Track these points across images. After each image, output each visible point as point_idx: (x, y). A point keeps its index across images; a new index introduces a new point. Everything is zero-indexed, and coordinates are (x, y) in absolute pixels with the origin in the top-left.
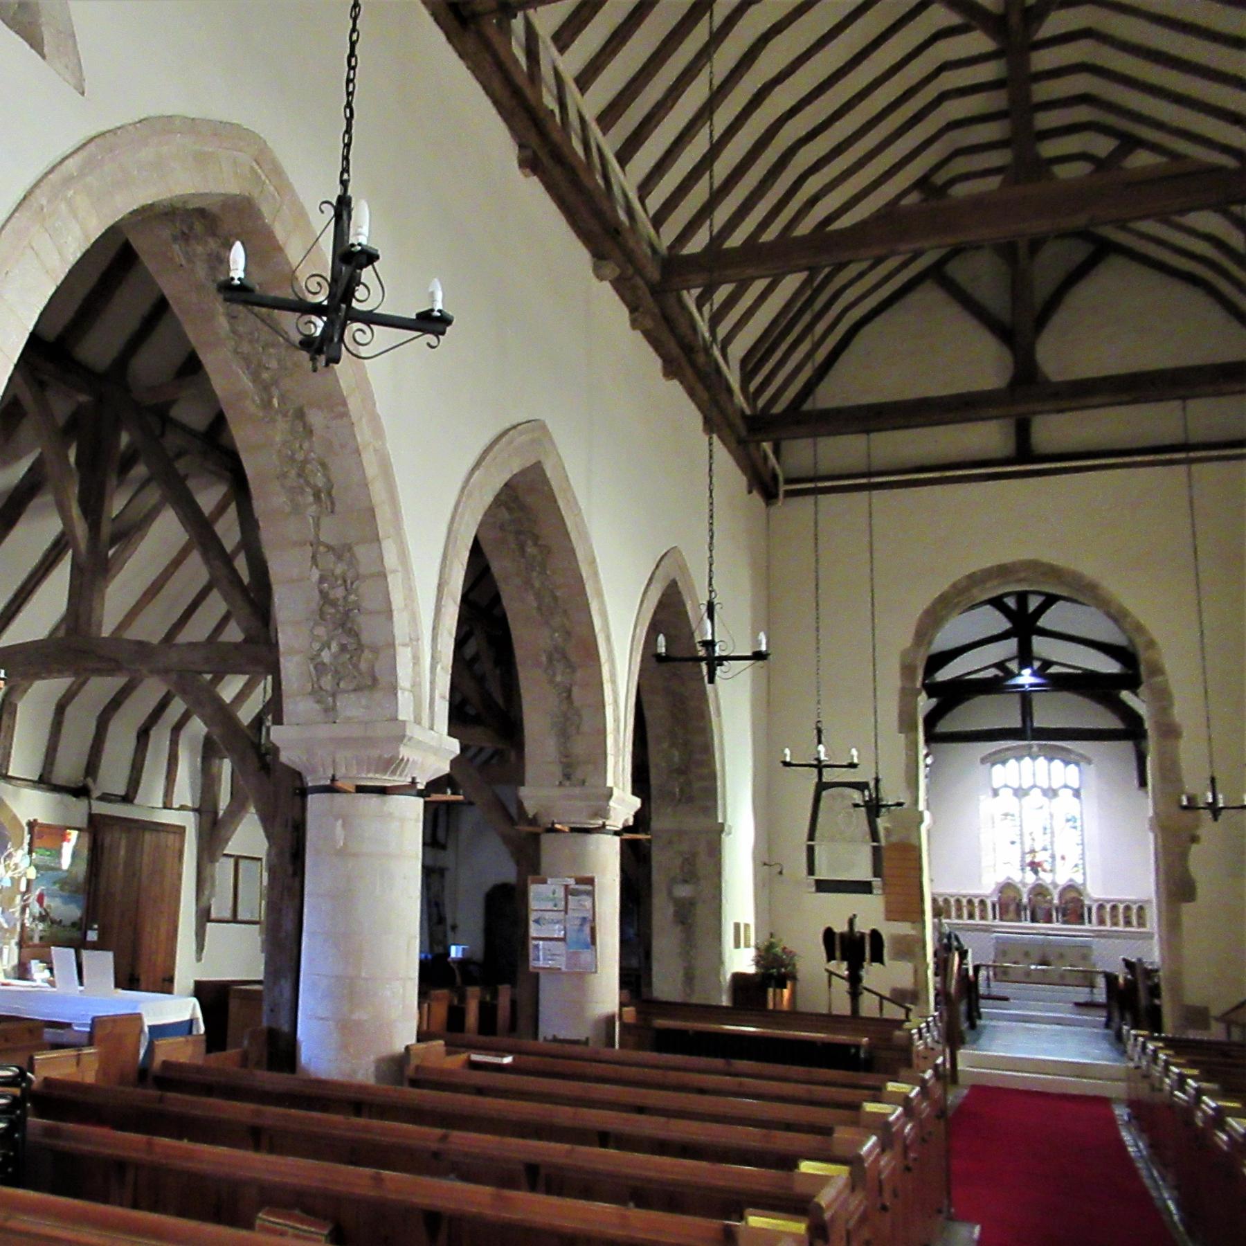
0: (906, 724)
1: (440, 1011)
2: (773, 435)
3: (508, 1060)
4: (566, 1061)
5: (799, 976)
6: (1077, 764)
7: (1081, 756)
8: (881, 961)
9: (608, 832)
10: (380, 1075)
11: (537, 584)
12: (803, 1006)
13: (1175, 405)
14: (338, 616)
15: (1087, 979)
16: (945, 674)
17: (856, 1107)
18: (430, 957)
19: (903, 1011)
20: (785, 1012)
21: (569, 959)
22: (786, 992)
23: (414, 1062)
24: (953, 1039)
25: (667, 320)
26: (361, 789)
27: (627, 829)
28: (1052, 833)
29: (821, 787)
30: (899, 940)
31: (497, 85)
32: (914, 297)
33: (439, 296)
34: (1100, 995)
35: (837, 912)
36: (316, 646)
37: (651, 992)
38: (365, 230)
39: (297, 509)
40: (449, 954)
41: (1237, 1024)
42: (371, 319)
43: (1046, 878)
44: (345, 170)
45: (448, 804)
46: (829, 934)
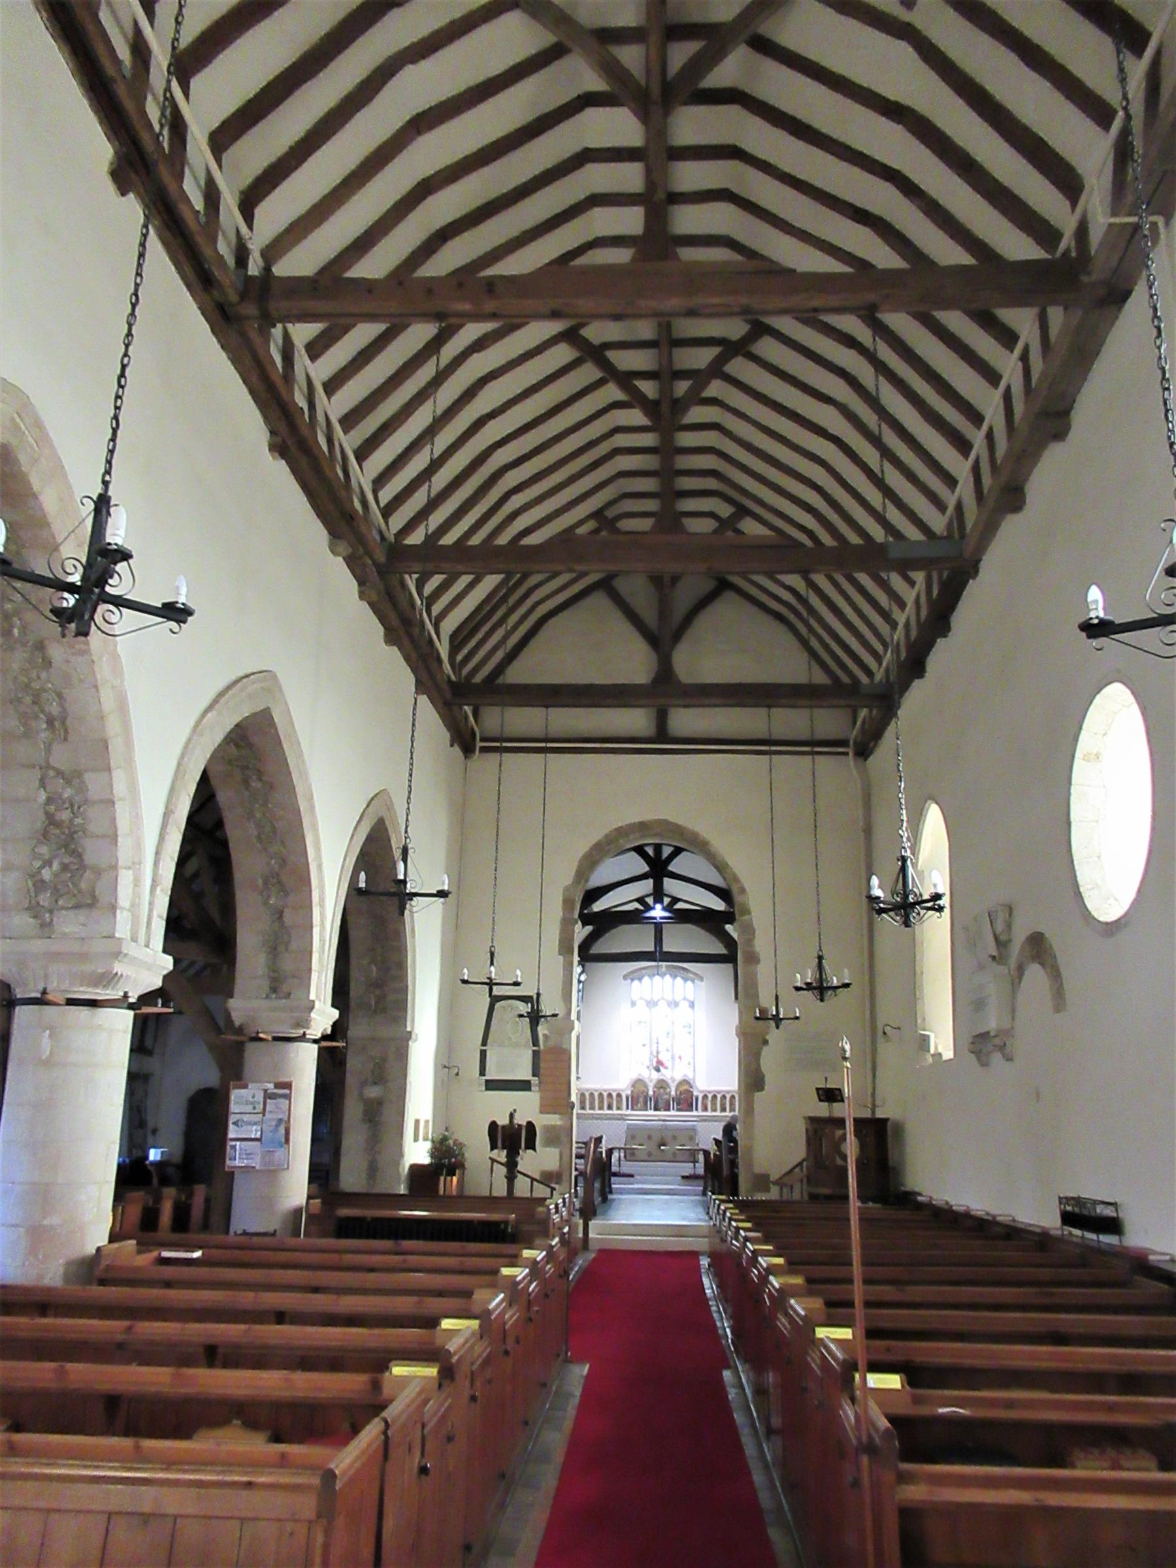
0: (565, 948)
1: (135, 1212)
2: (472, 700)
3: (197, 1254)
4: (257, 1252)
5: (467, 1165)
6: (693, 981)
7: (696, 974)
8: (534, 1149)
9: (308, 1041)
10: (67, 1278)
11: (258, 815)
12: (471, 1191)
13: (763, 711)
14: (63, 837)
15: (692, 1156)
16: (598, 906)
17: (495, 1272)
18: (127, 1161)
19: (549, 1190)
20: (454, 1197)
21: (263, 1158)
22: (455, 1179)
23: (104, 1263)
24: (588, 1212)
25: (390, 596)
26: (71, 1002)
27: (325, 1037)
28: (674, 1038)
29: (495, 1000)
30: (549, 1129)
31: (254, 379)
32: (586, 602)
33: (184, 591)
34: (700, 1170)
35: (503, 1107)
36: (37, 864)
37: (338, 1185)
38: (122, 532)
39: (29, 734)
40: (147, 1157)
41: (786, 1185)
42: (120, 602)
43: (666, 1074)
44: (108, 472)
45: (158, 1015)
46: (493, 1126)
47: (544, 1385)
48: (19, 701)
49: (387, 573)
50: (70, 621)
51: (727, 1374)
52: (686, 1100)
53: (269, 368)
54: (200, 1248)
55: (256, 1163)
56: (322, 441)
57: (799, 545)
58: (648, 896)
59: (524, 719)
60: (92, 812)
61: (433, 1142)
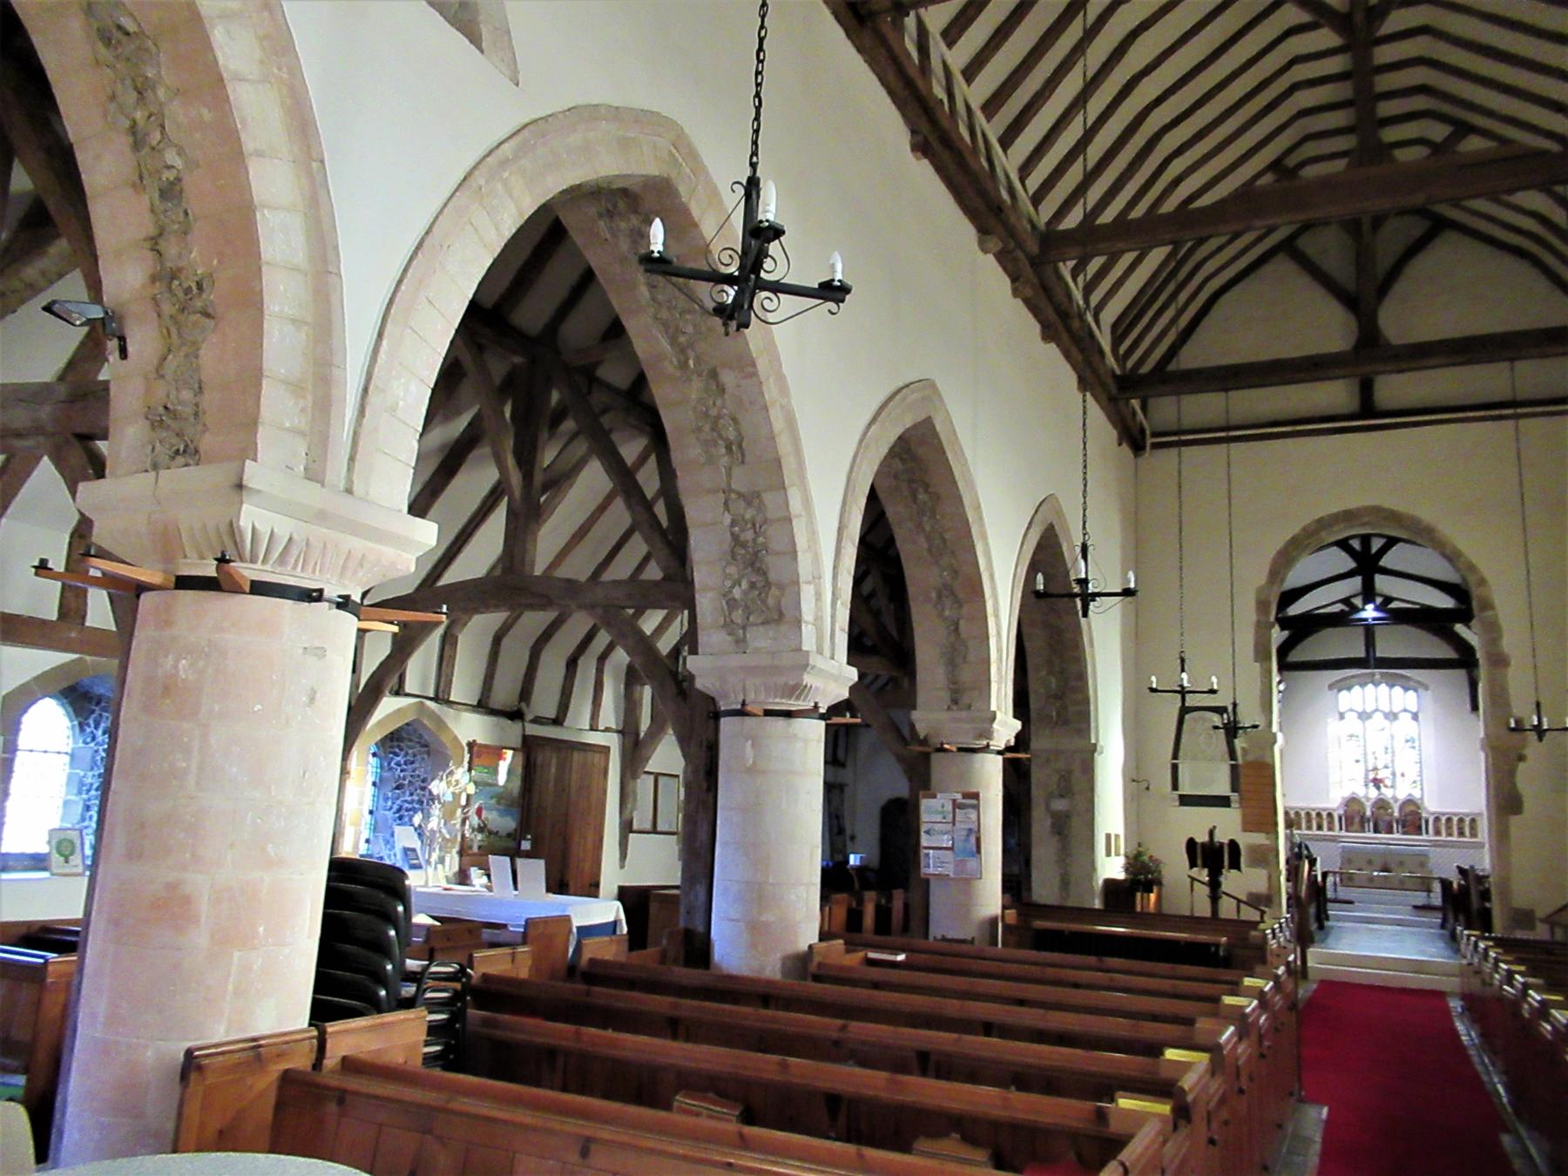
0: (1261, 654)
1: (840, 913)
2: (1140, 393)
3: (901, 957)
4: (954, 959)
8: (1238, 868)
9: (992, 752)
11: (928, 528)
12: (1167, 909)
15: (1425, 885)
16: (1295, 609)
17: (1216, 1000)
22: (1153, 896)
23: (817, 959)
24: (1304, 938)
25: (1045, 289)
26: (768, 713)
27: (1008, 749)
29: (1184, 710)
32: (1268, 269)
33: (839, 267)
34: (1436, 899)
35: (1199, 824)
36: (728, 583)
38: (772, 208)
39: (711, 460)
41: (1560, 925)
42: (778, 288)
43: (1387, 793)
44: (755, 153)
45: (847, 725)
46: (1191, 844)
47: (1280, 1126)
48: (699, 429)
49: (1037, 264)
50: (731, 317)
51: (1506, 1140)
52: (1413, 824)
53: (902, 58)
54: (903, 951)
55: (949, 870)
56: (964, 132)
57: (1542, 154)
58: (1355, 596)
59: (1204, 407)
60: (771, 530)
61: (1127, 856)
